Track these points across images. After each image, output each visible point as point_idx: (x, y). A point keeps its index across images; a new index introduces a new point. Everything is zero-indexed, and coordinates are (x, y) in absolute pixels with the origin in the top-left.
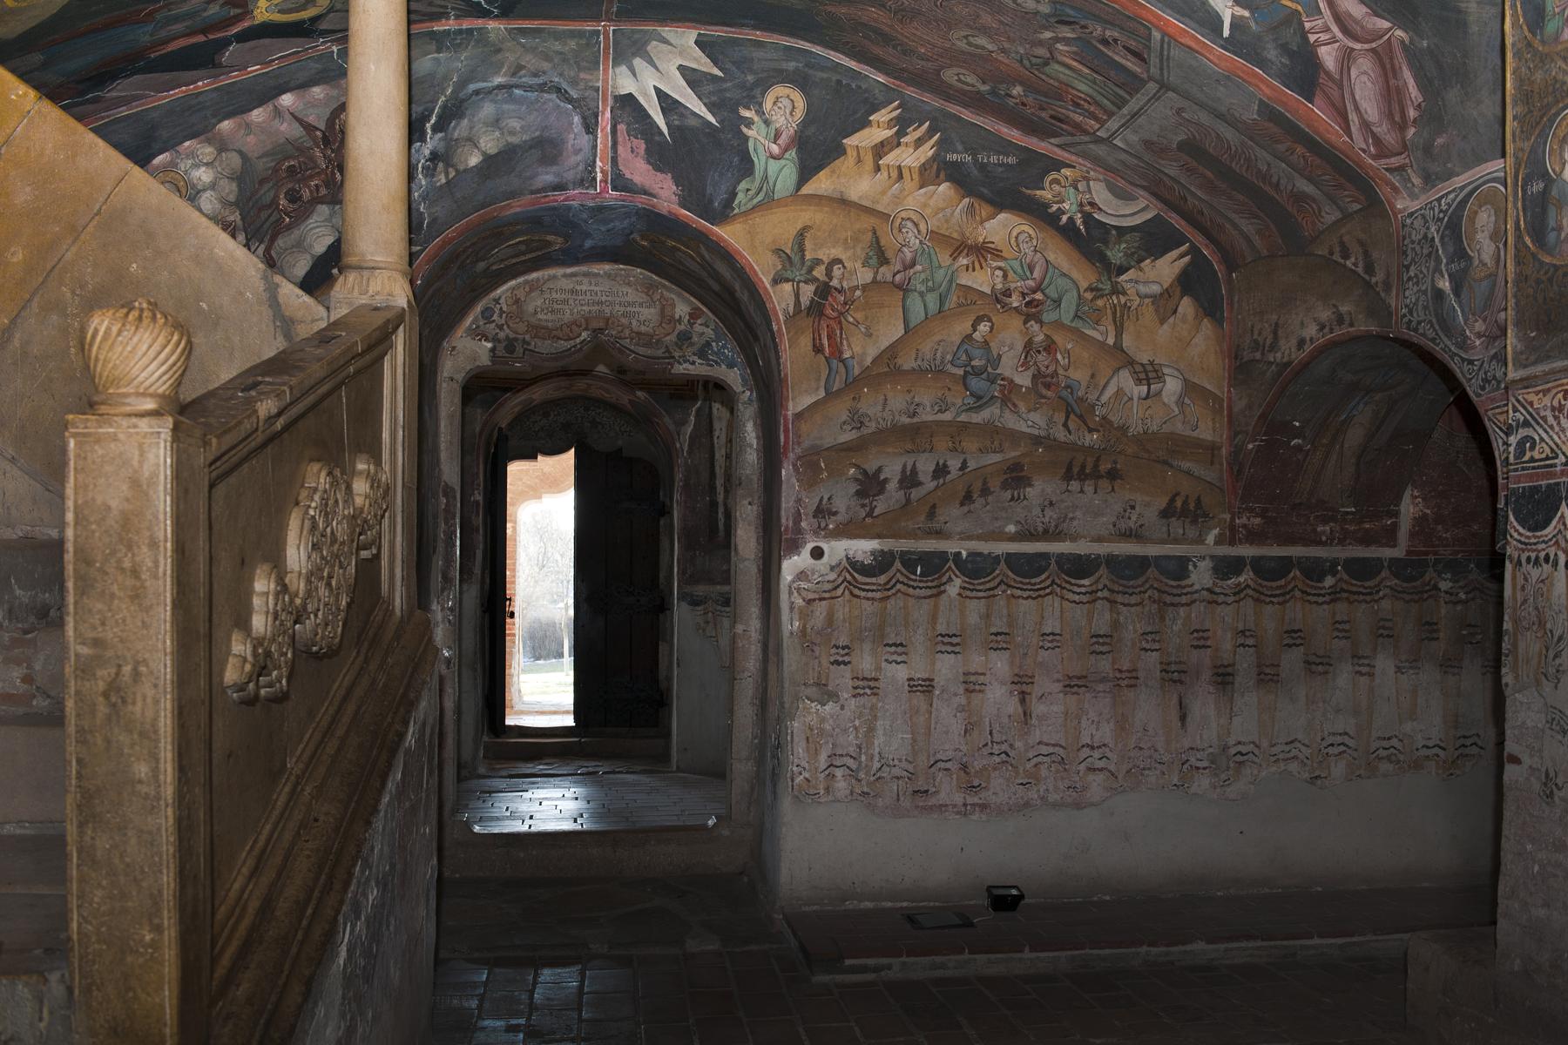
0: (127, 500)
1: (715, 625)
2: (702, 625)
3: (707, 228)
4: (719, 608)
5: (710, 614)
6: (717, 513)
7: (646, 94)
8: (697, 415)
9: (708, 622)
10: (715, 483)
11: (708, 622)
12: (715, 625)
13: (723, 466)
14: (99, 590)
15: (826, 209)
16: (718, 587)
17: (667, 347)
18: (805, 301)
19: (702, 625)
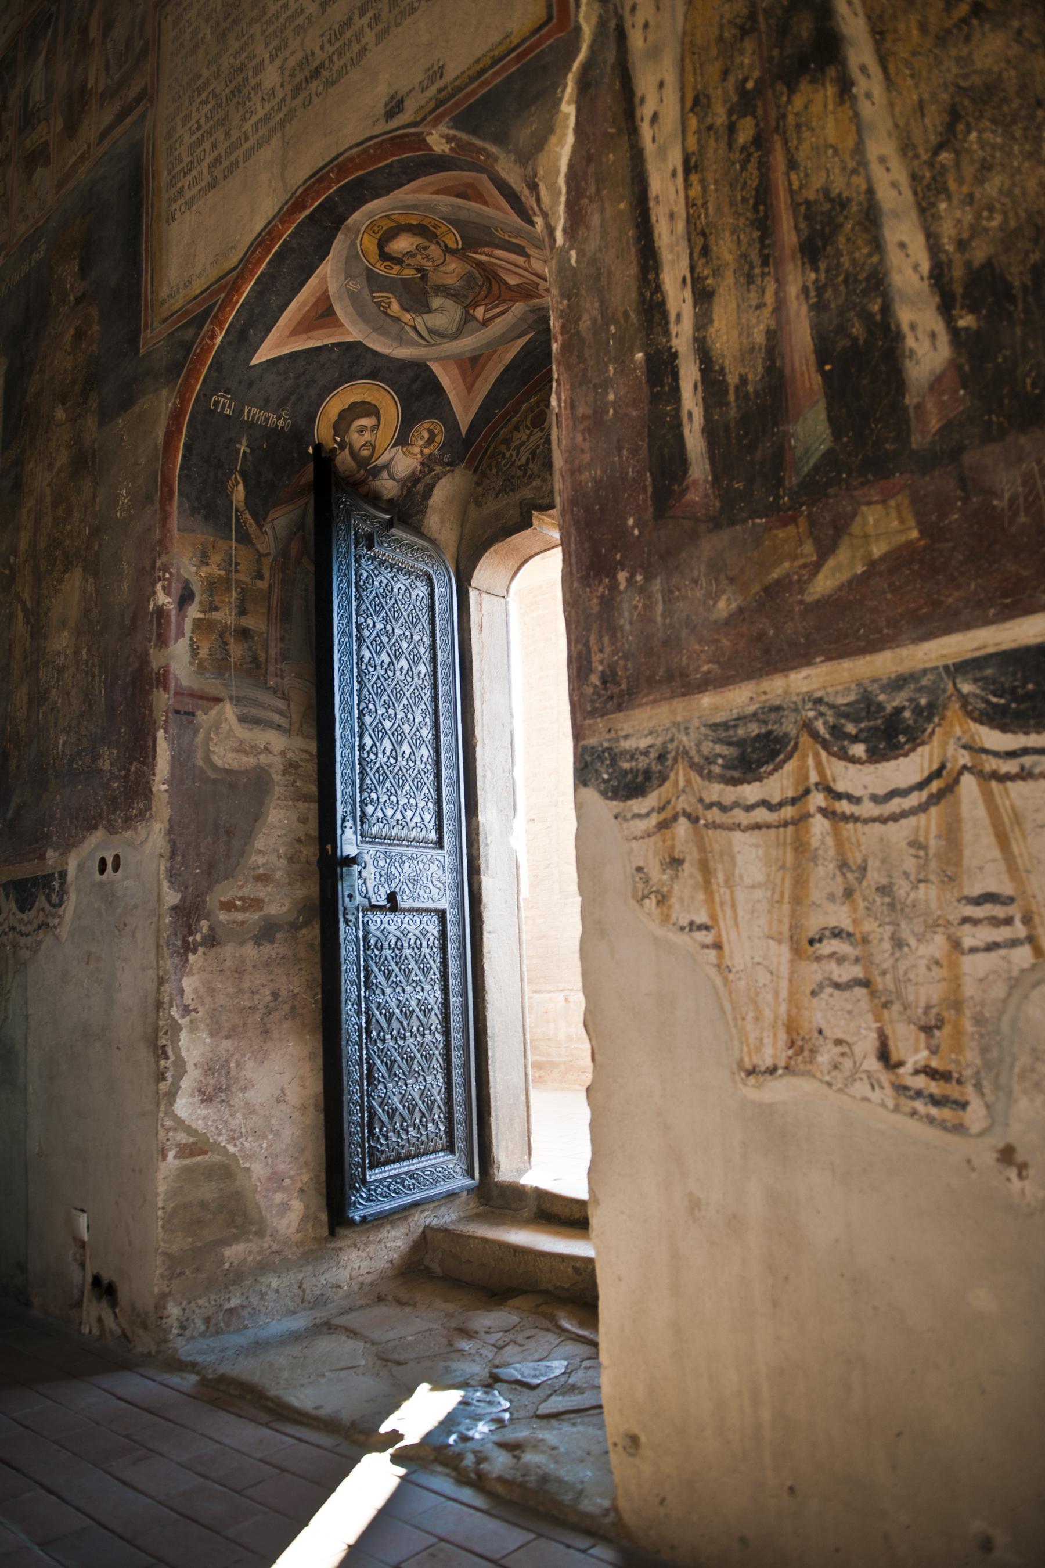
0: (217, 1324)
1: (705, 868)
2: (656, 874)
3: (567, 127)
4: (716, 791)
5: (683, 826)
6: (676, 391)
7: (454, 296)
8: (584, 86)
9: (675, 862)
10: (658, 288)
11: (675, 862)
12: (705, 868)
13: (681, 209)
14: (171, 1154)
15: (818, 660)
16: (706, 700)
17: (502, 1445)
18: (822, 658)
19: (656, 874)
